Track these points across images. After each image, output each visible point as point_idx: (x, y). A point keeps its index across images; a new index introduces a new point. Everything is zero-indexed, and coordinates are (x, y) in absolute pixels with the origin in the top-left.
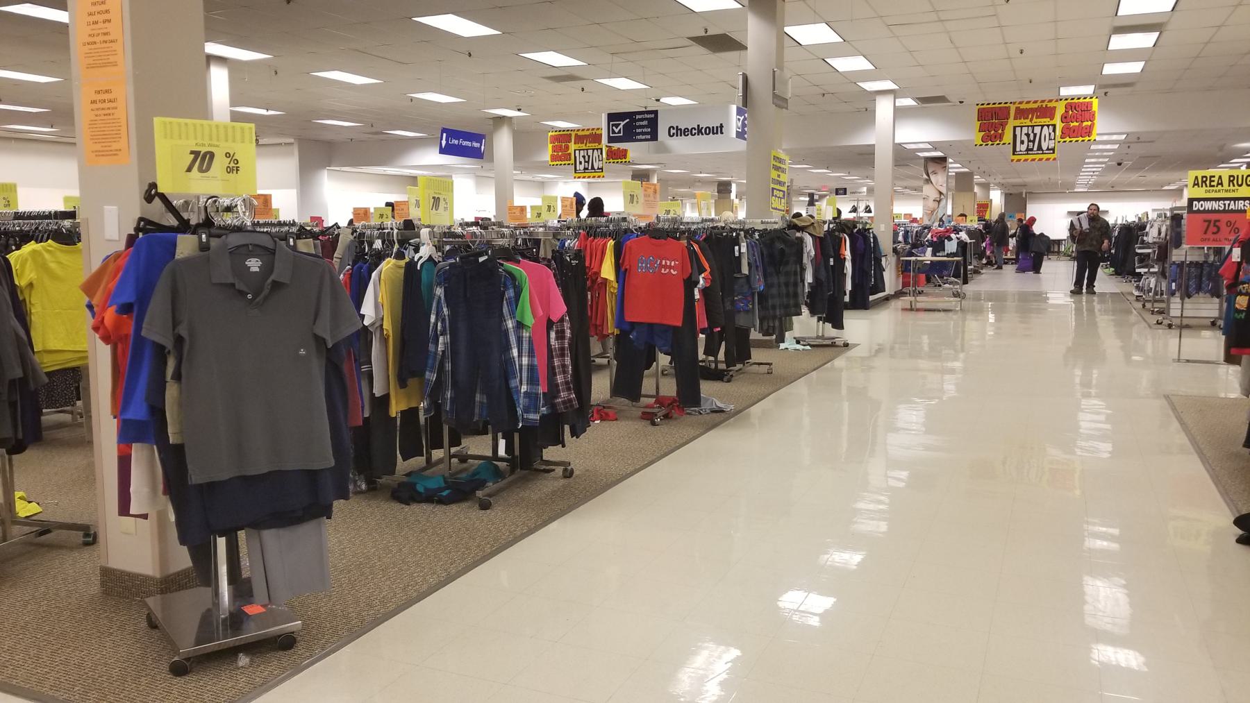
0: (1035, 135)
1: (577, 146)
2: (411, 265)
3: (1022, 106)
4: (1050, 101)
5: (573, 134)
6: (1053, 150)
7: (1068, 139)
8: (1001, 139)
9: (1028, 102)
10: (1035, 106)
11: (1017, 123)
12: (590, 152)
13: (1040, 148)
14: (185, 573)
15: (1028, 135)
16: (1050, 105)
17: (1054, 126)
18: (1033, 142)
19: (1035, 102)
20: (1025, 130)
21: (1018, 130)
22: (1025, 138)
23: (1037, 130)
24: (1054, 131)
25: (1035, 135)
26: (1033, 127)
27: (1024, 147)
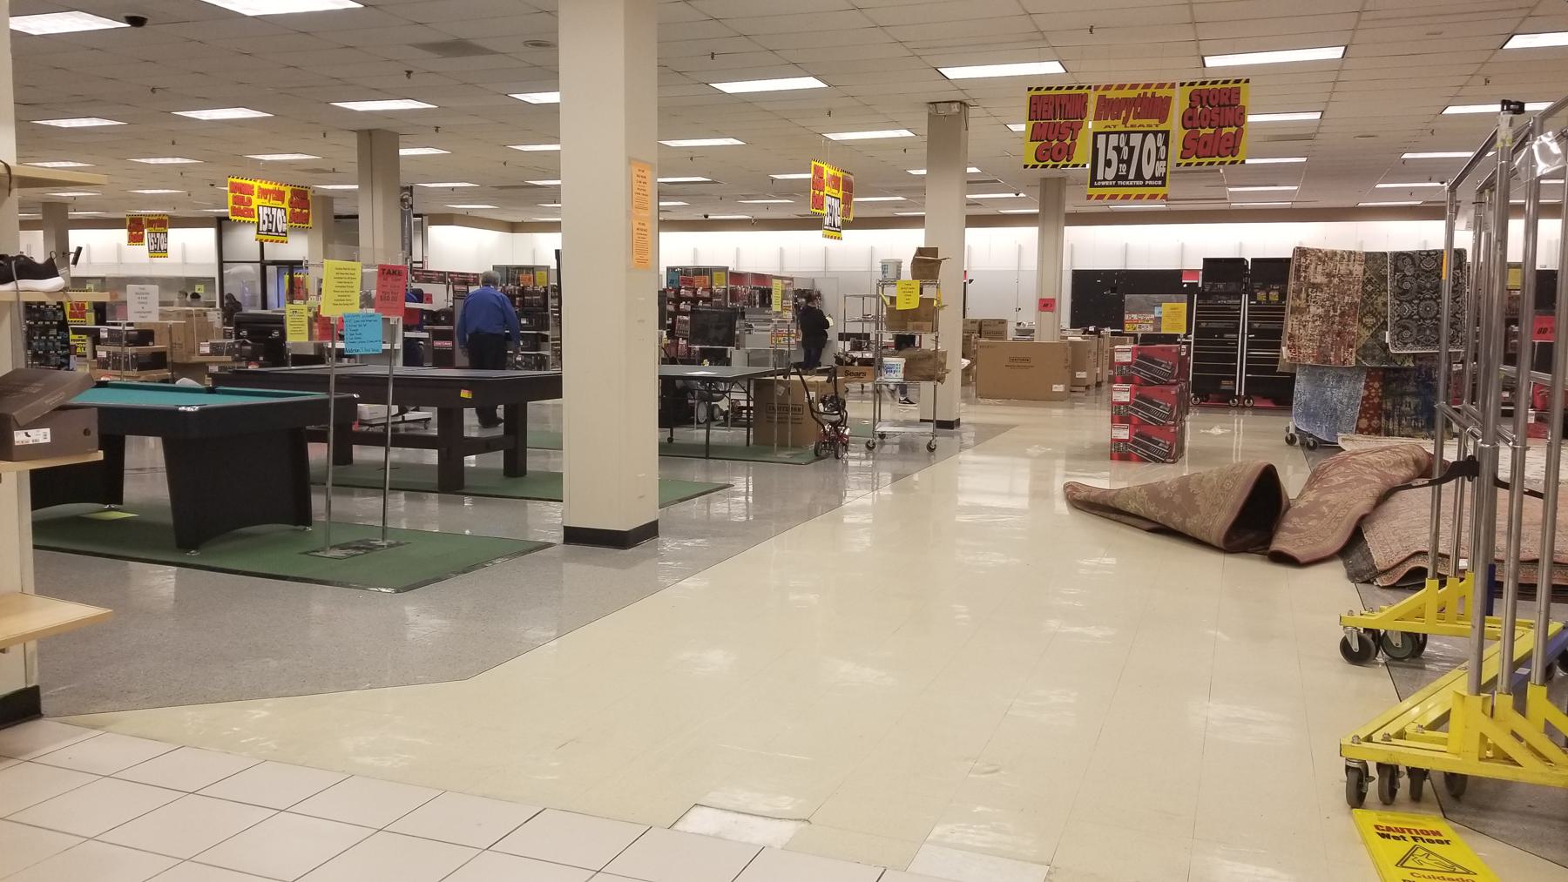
0: (1131, 150)
1: (1101, 126)
3: (1111, 94)
4: (1161, 86)
7: (1194, 160)
8: (1070, 156)
10: (1133, 94)
11: (1101, 126)
13: (1139, 175)
15: (1118, 149)
16: (1160, 93)
17: (1166, 133)
18: (1128, 162)
19: (1134, 87)
20: (1113, 140)
21: (1101, 139)
22: (1113, 155)
23: (1136, 140)
24: (1166, 143)
25: (1131, 150)
26: (1128, 133)
27: (1111, 173)
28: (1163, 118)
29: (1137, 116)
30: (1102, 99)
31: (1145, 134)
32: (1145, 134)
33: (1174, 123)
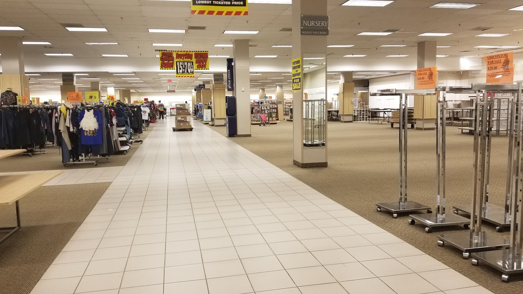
1: (178, 60)
2: (190, 114)
3: (179, 53)
4: (190, 51)
5: (193, 53)
6: (193, 72)
9: (181, 51)
10: (184, 53)
12: (186, 64)
13: (187, 72)
14: (367, 103)
15: (182, 65)
16: (190, 53)
17: (192, 62)
18: (185, 69)
19: (184, 51)
20: (181, 63)
21: (178, 63)
22: (181, 67)
23: (186, 64)
27: (181, 71)
28: (191, 59)
29: (186, 58)
30: (177, 54)
31: (188, 62)
32: (188, 62)
33: (194, 60)
